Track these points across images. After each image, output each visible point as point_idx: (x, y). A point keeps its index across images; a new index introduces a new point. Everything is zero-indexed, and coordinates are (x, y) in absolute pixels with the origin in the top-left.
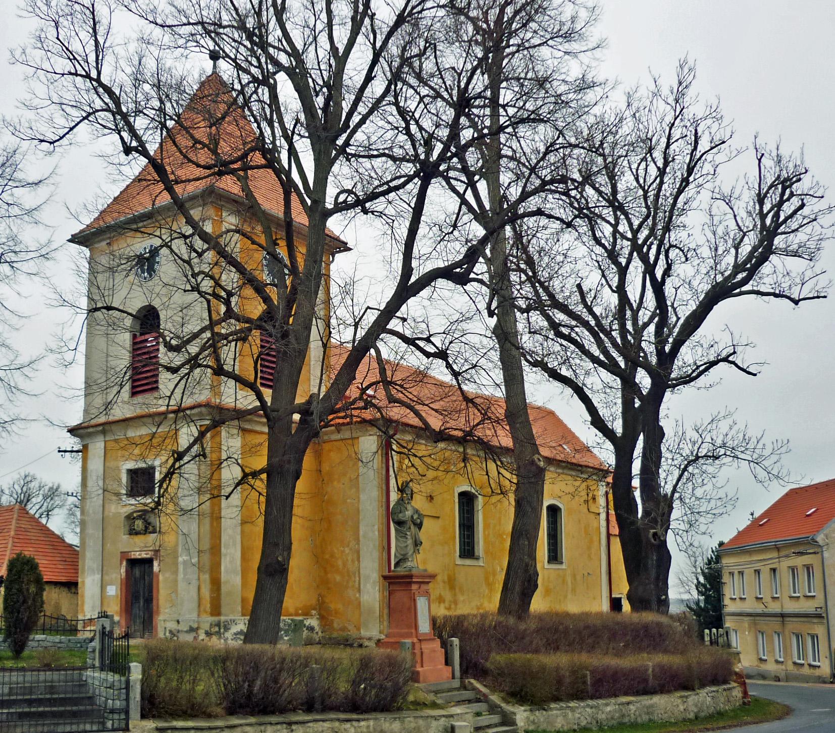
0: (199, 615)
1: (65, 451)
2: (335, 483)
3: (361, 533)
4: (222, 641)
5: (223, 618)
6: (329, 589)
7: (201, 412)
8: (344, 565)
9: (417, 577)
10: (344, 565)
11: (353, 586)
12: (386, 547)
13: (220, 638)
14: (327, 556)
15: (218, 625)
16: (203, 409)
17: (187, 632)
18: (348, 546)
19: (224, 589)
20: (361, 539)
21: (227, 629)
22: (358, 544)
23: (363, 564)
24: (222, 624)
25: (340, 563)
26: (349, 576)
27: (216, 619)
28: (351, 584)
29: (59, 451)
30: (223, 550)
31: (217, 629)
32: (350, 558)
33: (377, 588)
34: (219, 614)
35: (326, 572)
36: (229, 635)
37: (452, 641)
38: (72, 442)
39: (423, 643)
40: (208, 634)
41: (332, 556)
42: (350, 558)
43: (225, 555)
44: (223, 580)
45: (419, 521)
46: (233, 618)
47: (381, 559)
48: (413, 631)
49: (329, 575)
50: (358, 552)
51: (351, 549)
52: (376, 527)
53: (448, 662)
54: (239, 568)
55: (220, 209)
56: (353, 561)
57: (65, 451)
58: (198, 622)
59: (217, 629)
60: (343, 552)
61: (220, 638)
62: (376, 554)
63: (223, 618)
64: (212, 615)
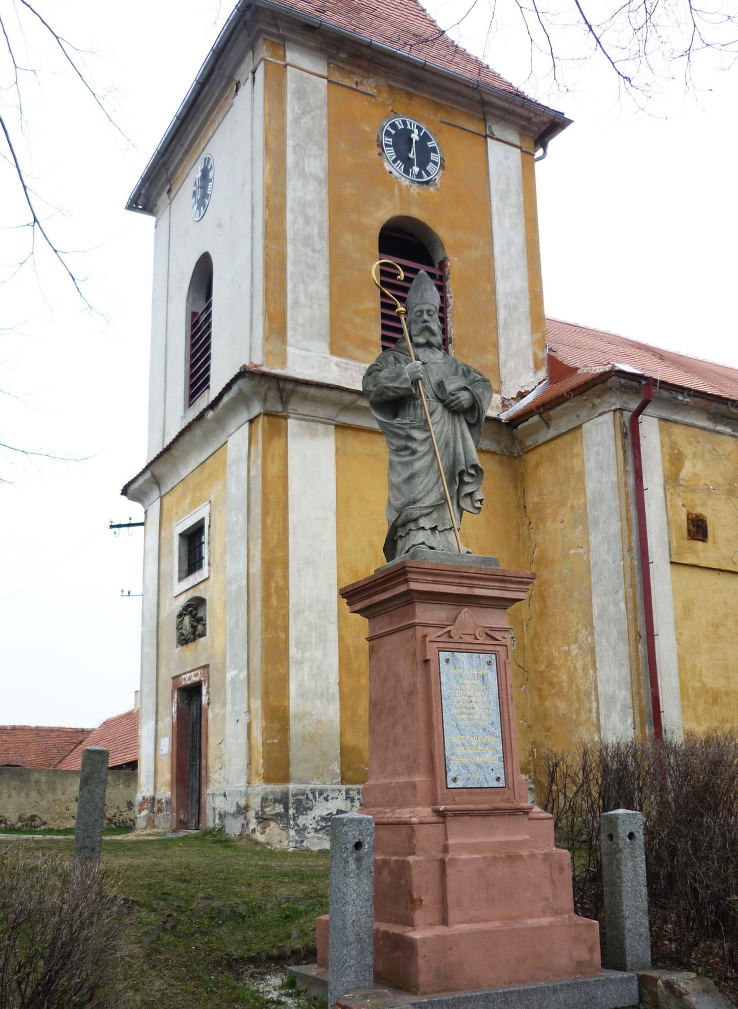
0: (249, 782)
1: (119, 526)
2: (549, 524)
3: (596, 610)
4: (292, 833)
5: (292, 787)
6: (548, 730)
7: (241, 392)
8: (571, 680)
9: (427, 572)
10: (571, 680)
11: (589, 719)
12: (644, 634)
13: (286, 827)
14: (542, 667)
15: (283, 799)
16: (241, 383)
17: (233, 815)
18: (575, 641)
19: (295, 728)
20: (596, 622)
21: (302, 807)
22: (592, 634)
23: (601, 675)
24: (291, 800)
25: (564, 677)
26: (579, 700)
27: (278, 788)
28: (584, 716)
29: (112, 527)
30: (293, 651)
31: (279, 809)
32: (579, 665)
33: (630, 720)
34: (286, 779)
35: (542, 698)
36: (305, 820)
37: (613, 820)
38: (134, 510)
39: (454, 825)
40: (263, 820)
41: (550, 665)
42: (579, 665)
43: (300, 662)
44: (293, 709)
45: (464, 397)
46: (320, 786)
47: (634, 657)
48: (420, 779)
49: (547, 704)
50: (592, 651)
51: (580, 647)
52: (621, 594)
53: (593, 894)
54: (335, 689)
55: (280, 44)
56: (585, 668)
57: (119, 526)
58: (247, 795)
59: (279, 809)
60: (568, 653)
61: (286, 827)
62: (624, 650)
63: (292, 787)
64: (267, 779)
